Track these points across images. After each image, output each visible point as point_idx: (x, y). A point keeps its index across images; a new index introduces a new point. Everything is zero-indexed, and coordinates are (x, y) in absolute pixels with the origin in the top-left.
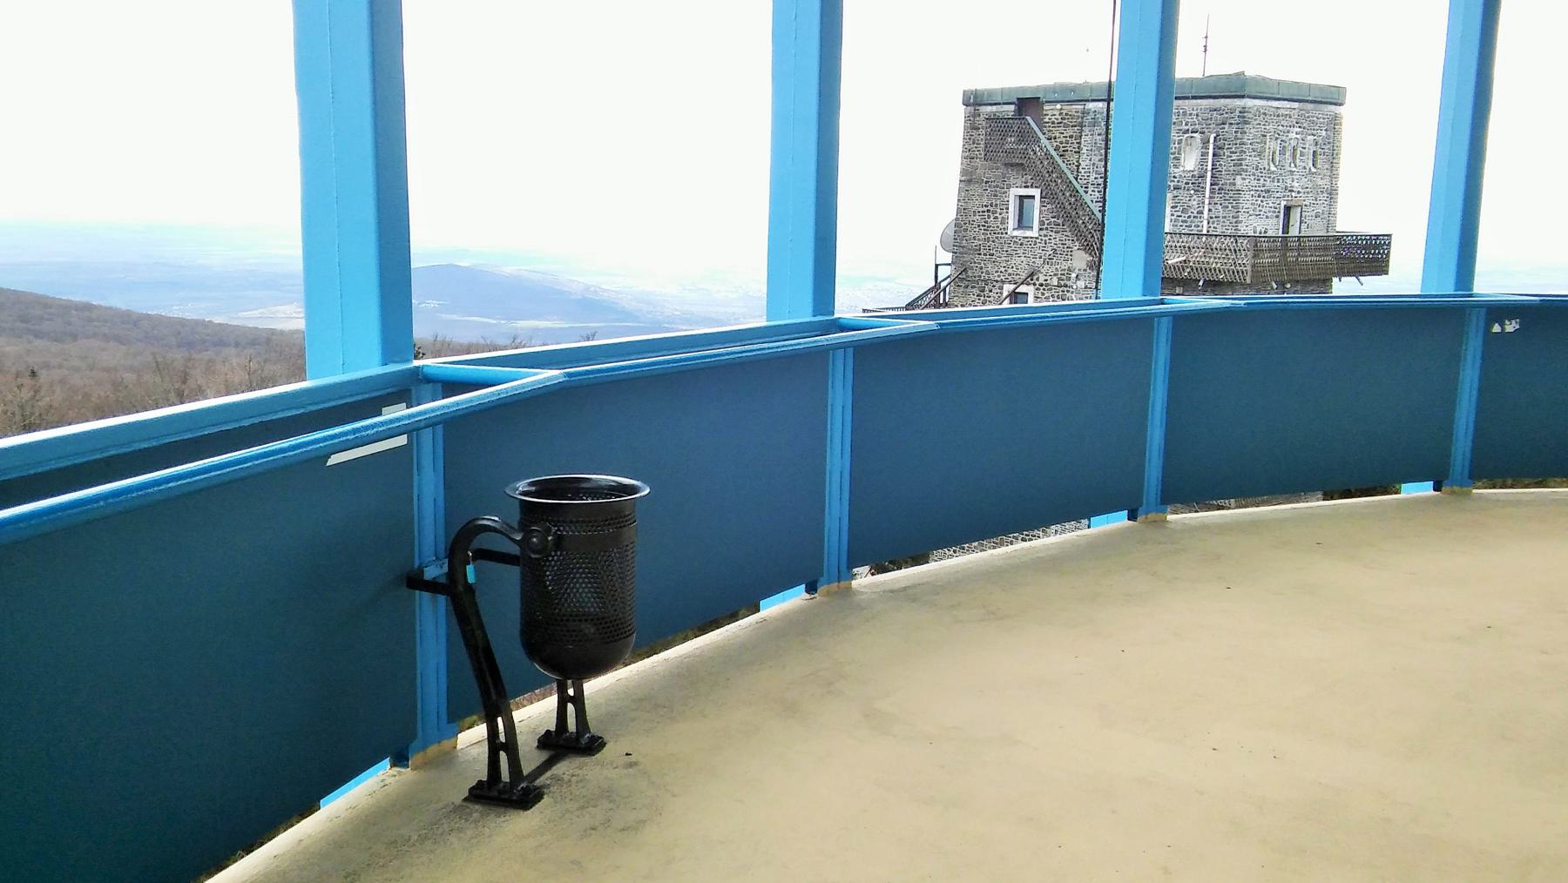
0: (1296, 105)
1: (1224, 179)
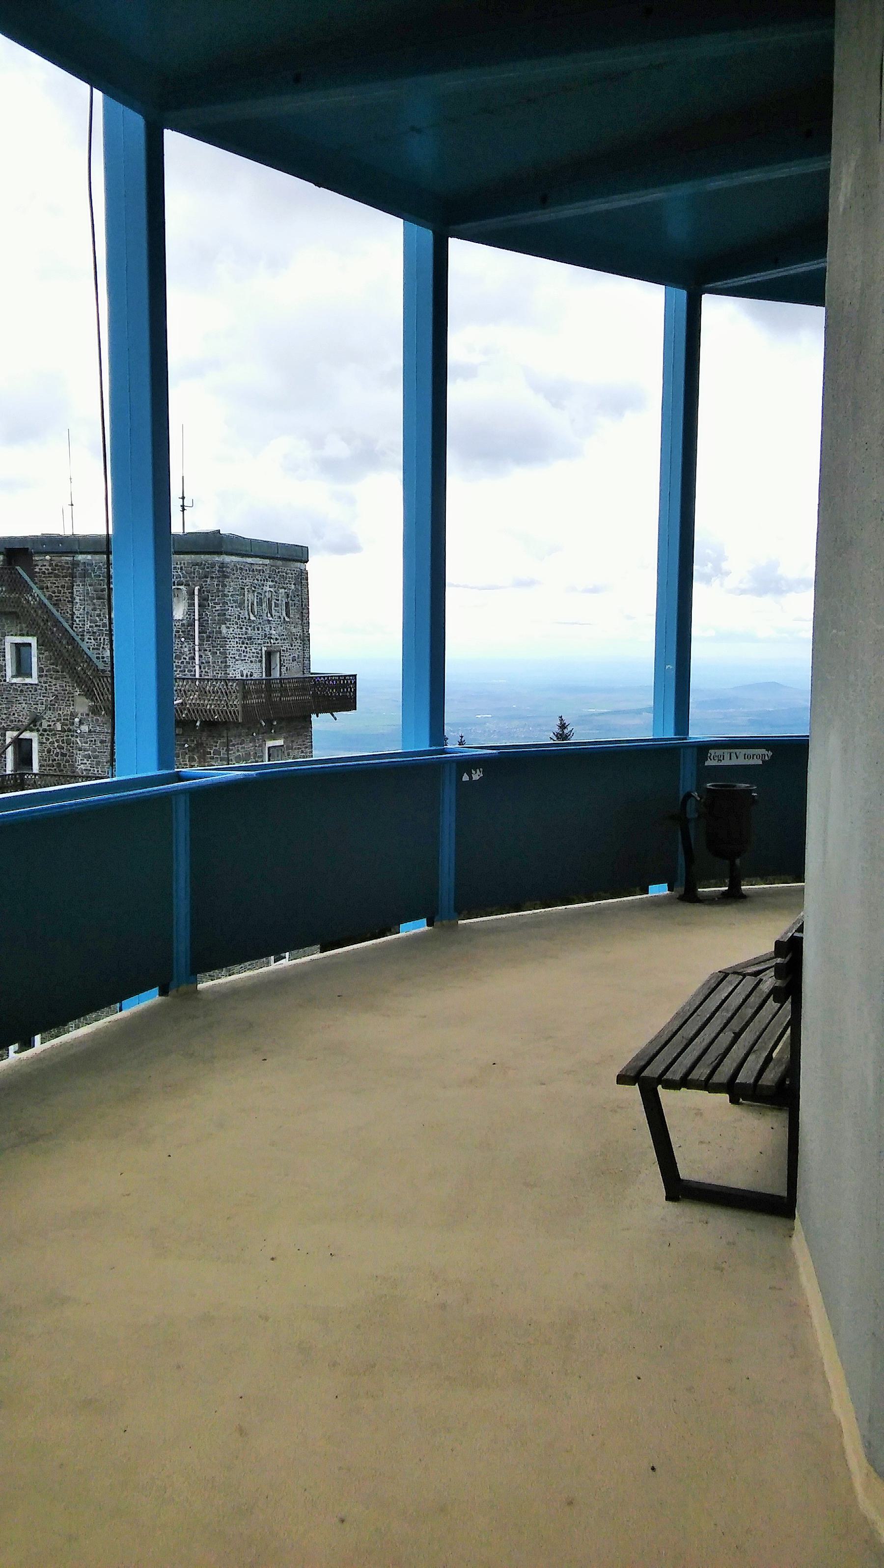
0: (267, 561)
1: (211, 627)
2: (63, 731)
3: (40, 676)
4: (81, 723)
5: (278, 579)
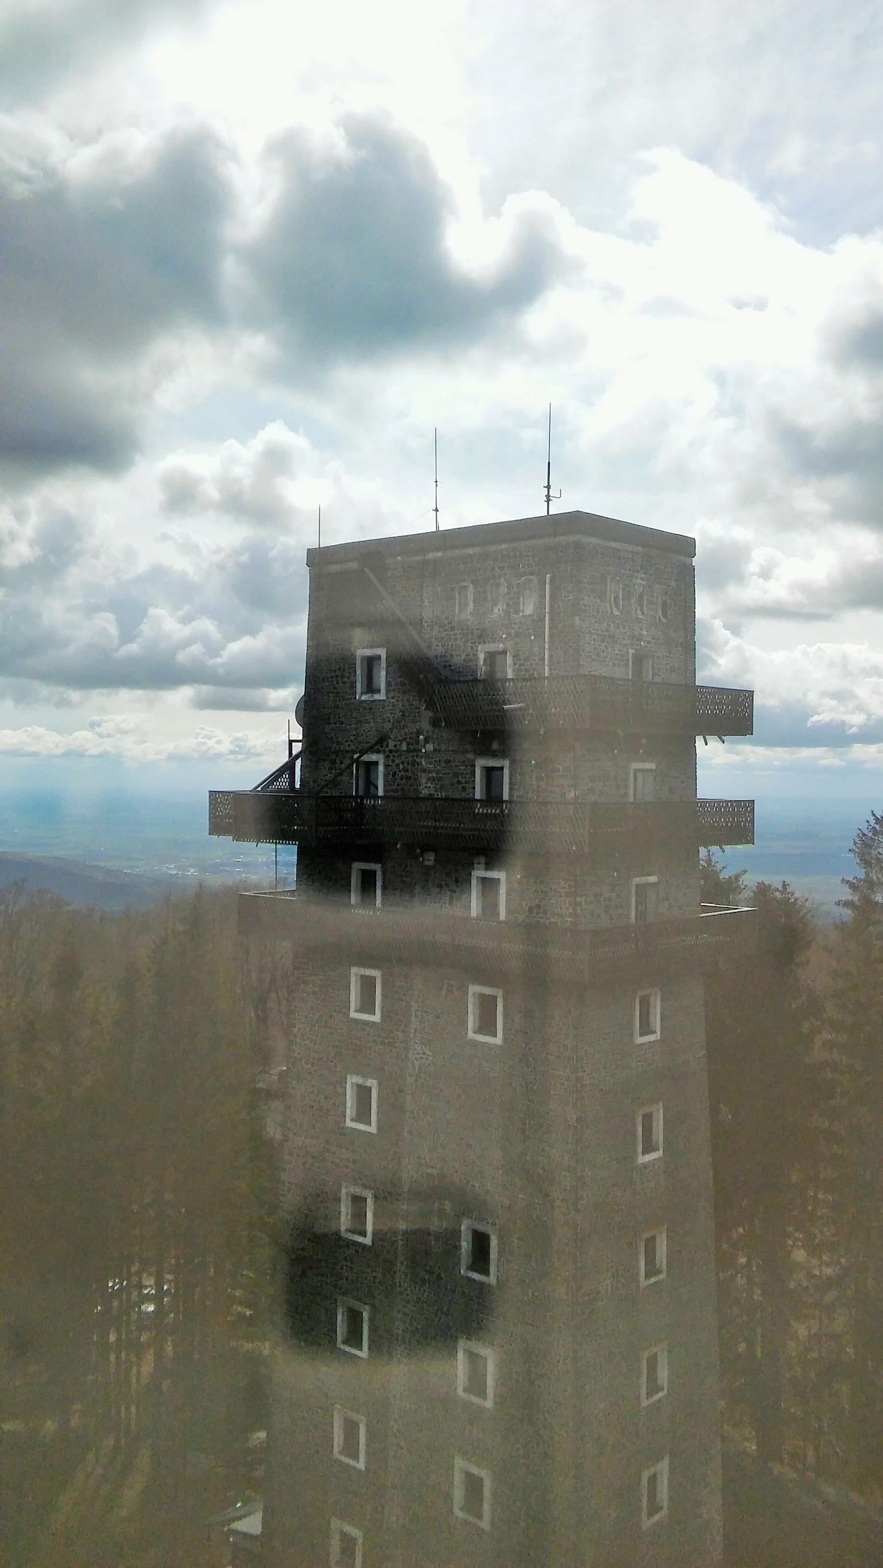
2: (409, 751)
3: (388, 691)
4: (426, 741)
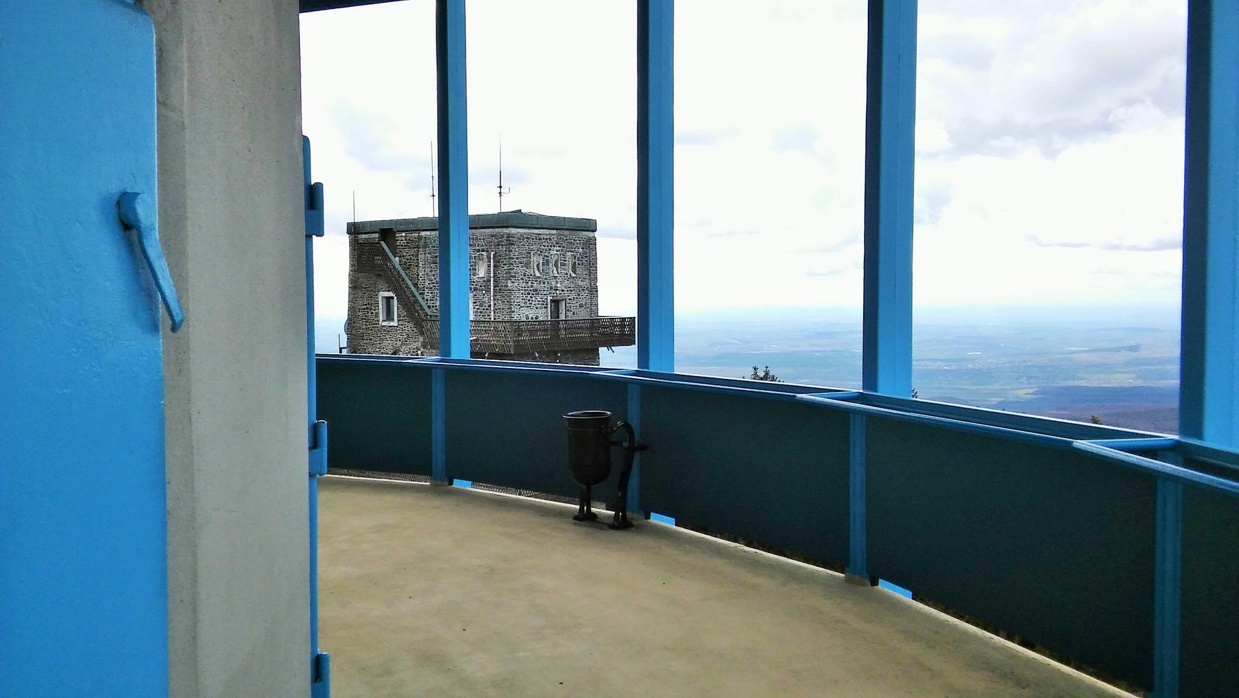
0: (554, 232)
5: (568, 245)
